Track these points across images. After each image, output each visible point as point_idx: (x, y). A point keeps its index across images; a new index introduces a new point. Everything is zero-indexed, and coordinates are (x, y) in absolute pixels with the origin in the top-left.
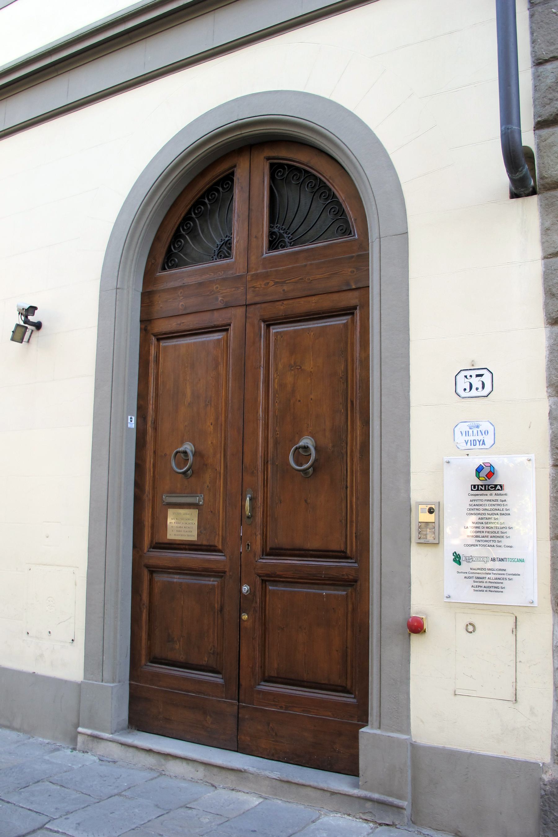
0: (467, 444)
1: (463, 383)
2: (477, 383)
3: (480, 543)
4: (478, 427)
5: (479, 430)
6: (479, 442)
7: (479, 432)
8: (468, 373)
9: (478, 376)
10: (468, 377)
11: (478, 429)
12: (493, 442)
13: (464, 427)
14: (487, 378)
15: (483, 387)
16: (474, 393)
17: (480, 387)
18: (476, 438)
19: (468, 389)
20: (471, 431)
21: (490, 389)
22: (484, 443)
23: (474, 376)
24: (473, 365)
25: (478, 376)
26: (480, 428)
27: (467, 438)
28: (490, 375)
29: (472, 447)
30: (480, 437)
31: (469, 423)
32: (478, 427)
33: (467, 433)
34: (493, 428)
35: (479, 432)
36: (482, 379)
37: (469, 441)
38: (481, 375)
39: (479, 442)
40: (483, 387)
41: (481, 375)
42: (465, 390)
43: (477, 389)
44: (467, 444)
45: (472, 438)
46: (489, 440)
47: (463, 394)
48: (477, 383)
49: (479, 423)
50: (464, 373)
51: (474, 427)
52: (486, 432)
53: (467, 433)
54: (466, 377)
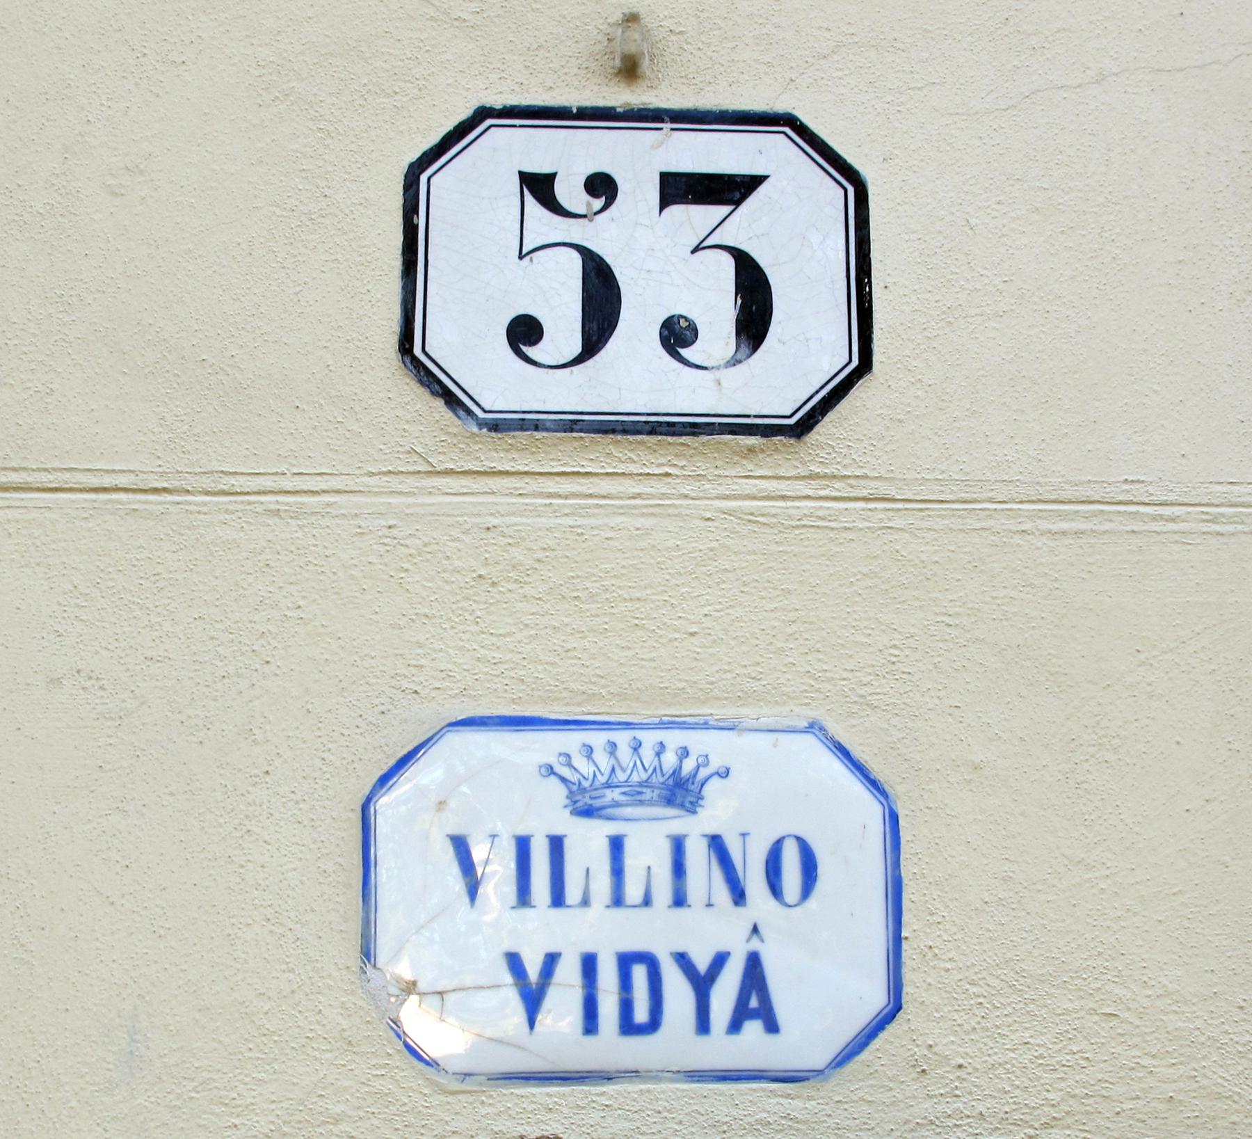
0: (533, 1000)
1: (493, 261)
2: (670, 264)
3: (1045, 525)
4: (681, 791)
5: (695, 828)
6: (702, 984)
7: (697, 854)
8: (570, 155)
9: (680, 189)
10: (570, 192)
11: (679, 823)
12: (877, 999)
13: (502, 787)
14: (794, 225)
15: (754, 321)
16: (632, 374)
17: (716, 312)
18: (658, 932)
19: (563, 335)
20: (587, 844)
21: (833, 356)
22: (756, 1004)
23: (638, 190)
24: (630, 70)
25: (680, 189)
26: (718, 812)
27: (539, 931)
28: (830, 196)
29: (609, 1046)
30: (710, 929)
31: (572, 740)
32: (681, 791)
33: (540, 870)
34: (384, 803)
35: (697, 854)
36: (744, 226)
37: (569, 972)
38: (729, 190)
39: (702, 984)
40: (754, 321)
41: (729, 190)
42: (524, 332)
43: (676, 336)
44: (533, 1000)
45: (599, 930)
46: (823, 969)
47: (499, 381)
48: (670, 264)
49: (698, 742)
50: (508, 151)
51: (636, 794)
52: (795, 867)
53: (540, 870)
54: (539, 186)
